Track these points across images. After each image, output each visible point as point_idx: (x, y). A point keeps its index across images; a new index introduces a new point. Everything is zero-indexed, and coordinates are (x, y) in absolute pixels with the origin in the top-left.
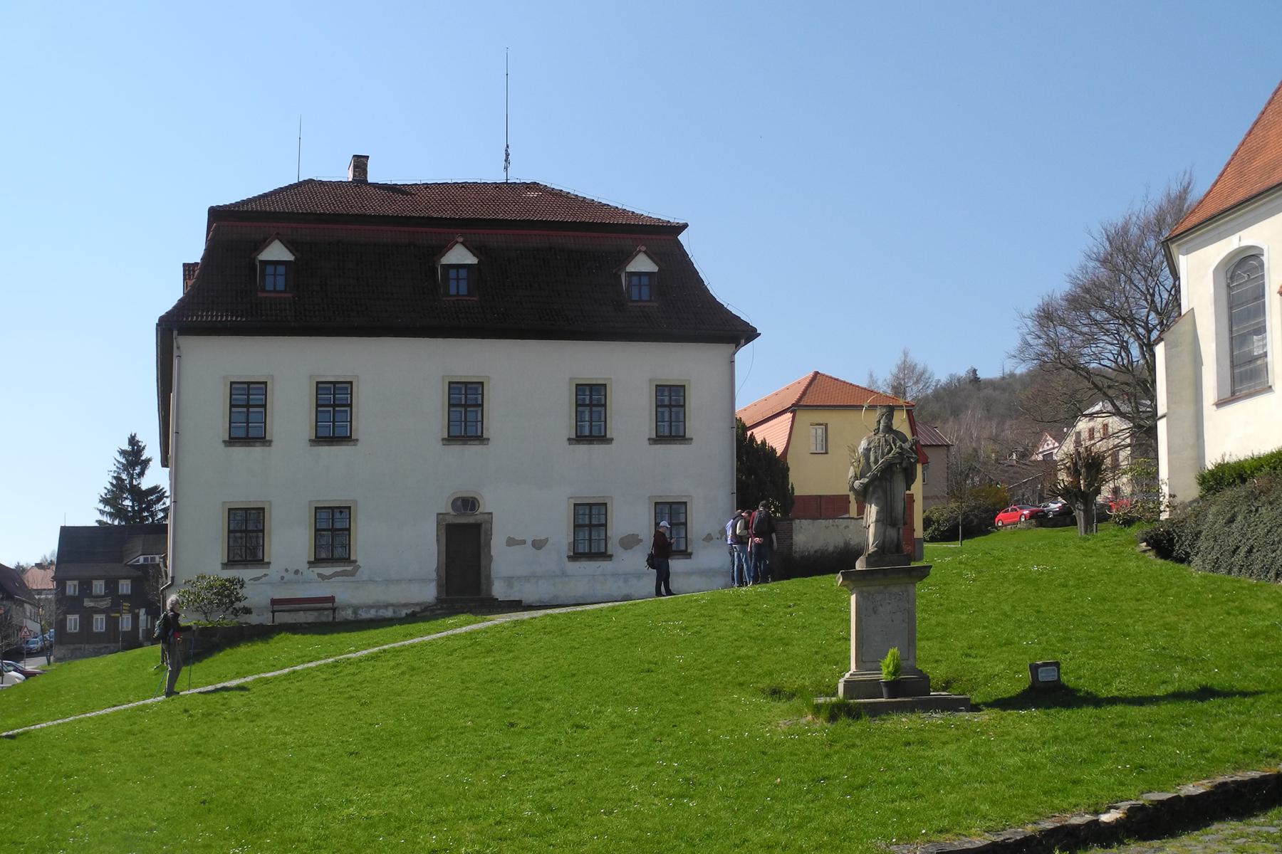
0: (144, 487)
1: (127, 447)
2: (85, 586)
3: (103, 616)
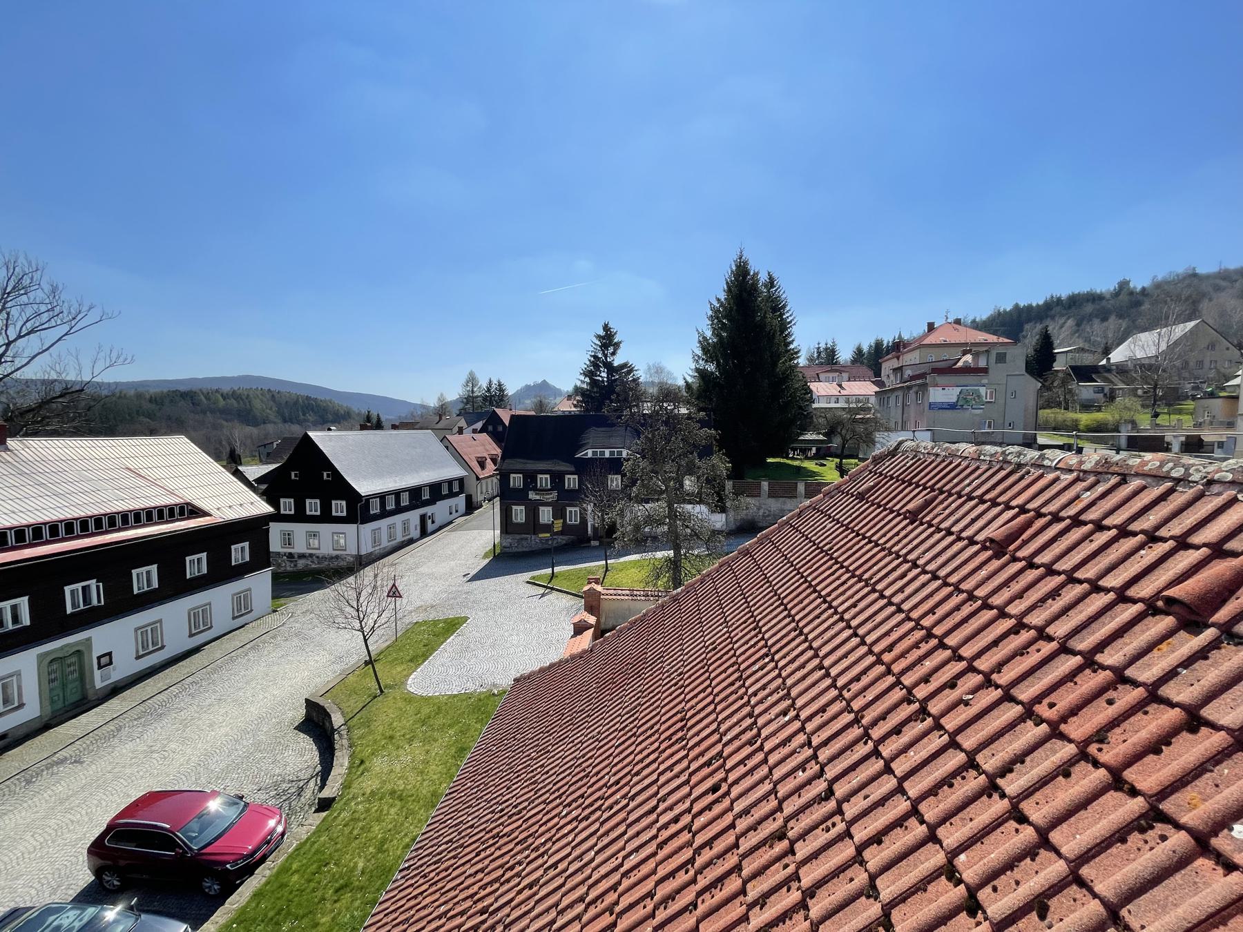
0: (616, 364)
1: (602, 333)
2: (530, 478)
3: (550, 509)
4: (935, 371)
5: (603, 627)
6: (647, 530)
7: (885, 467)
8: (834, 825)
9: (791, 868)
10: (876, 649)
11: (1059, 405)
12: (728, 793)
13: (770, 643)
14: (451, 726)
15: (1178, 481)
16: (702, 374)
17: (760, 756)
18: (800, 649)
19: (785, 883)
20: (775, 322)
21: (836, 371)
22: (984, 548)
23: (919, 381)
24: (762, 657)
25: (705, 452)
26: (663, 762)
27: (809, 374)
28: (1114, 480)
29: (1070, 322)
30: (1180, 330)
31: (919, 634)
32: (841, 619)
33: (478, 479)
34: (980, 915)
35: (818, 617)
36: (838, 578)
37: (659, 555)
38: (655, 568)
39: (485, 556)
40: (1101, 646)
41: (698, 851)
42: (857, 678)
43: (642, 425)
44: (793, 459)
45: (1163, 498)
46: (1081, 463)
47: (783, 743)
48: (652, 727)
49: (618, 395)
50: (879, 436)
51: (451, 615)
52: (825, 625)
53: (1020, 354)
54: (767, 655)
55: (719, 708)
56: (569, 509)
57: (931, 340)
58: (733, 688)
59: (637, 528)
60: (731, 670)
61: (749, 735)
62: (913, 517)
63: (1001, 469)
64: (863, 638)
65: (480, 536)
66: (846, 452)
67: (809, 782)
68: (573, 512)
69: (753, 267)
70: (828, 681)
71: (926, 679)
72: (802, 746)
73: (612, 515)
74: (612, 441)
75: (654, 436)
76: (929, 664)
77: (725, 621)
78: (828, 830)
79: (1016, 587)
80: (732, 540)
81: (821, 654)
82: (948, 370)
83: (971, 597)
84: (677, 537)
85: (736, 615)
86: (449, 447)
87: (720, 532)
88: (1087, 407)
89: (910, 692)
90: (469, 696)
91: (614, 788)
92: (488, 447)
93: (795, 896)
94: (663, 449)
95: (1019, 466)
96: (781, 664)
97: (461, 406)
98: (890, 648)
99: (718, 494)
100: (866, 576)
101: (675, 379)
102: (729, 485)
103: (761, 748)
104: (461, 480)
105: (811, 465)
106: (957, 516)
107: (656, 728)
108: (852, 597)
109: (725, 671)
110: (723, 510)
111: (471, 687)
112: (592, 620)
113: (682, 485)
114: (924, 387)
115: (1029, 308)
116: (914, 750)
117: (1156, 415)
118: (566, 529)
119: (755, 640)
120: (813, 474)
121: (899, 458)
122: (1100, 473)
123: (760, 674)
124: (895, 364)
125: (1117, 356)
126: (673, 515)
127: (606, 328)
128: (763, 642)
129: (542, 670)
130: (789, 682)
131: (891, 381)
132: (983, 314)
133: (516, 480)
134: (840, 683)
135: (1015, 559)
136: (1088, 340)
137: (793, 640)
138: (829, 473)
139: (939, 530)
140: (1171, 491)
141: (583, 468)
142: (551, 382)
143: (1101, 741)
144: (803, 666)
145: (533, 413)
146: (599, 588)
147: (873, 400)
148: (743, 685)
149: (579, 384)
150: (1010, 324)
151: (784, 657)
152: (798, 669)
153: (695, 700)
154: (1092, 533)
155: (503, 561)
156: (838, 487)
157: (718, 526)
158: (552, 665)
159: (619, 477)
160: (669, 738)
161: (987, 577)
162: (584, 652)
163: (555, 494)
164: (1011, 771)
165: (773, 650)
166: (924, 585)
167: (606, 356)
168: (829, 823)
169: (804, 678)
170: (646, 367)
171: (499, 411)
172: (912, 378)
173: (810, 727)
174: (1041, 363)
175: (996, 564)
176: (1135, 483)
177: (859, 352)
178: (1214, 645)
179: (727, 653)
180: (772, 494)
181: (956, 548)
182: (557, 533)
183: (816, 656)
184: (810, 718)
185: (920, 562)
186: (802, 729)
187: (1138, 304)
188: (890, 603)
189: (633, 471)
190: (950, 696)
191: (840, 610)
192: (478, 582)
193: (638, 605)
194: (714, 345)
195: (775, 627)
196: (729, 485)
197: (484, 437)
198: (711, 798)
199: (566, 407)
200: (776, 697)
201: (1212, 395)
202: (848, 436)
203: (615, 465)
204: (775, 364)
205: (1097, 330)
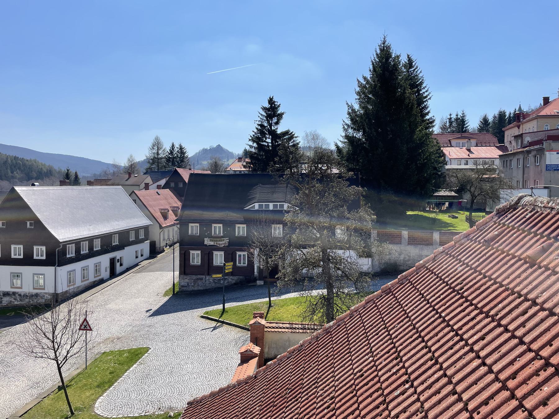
0: (279, 132)
1: (267, 105)
3: (222, 253)
5: (266, 356)
6: (304, 271)
10: (502, 376)
13: (410, 370)
16: (350, 140)
18: (436, 376)
23: (537, 147)
24: (403, 383)
27: (442, 140)
31: (538, 363)
32: (472, 350)
33: (161, 227)
35: (451, 348)
36: (468, 314)
37: (315, 293)
39: (166, 294)
50: (503, 193)
51: (134, 345)
54: (407, 381)
56: (238, 253)
58: (377, 411)
59: (296, 270)
65: (160, 278)
74: (275, 196)
75: (310, 192)
80: (377, 281)
81: (454, 380)
84: (330, 277)
85: (380, 346)
86: (137, 200)
87: (366, 274)
92: (171, 201)
94: (318, 202)
96: (419, 389)
97: (148, 166)
98: (513, 376)
101: (328, 144)
104: (146, 228)
108: (480, 330)
109: (370, 395)
112: (257, 350)
114: (541, 151)
119: (397, 368)
120: (447, 225)
124: (516, 132)
127: (271, 101)
128: (403, 370)
130: (427, 405)
131: (513, 146)
133: (194, 229)
134: (471, 406)
137: (430, 368)
144: (438, 392)
145: (209, 172)
146: (263, 322)
147: (497, 162)
148: (387, 408)
149: (248, 148)
151: (422, 383)
155: (181, 298)
158: (221, 390)
159: (281, 226)
162: (250, 378)
165: (413, 377)
166: (542, 321)
169: (439, 402)
171: (180, 170)
172: (531, 144)
177: (485, 121)
179: (372, 379)
182: (227, 274)
183: (450, 382)
188: (513, 337)
191: (470, 342)
194: (361, 116)
195: (414, 357)
197: (167, 191)
199: (238, 167)
204: (413, 132)
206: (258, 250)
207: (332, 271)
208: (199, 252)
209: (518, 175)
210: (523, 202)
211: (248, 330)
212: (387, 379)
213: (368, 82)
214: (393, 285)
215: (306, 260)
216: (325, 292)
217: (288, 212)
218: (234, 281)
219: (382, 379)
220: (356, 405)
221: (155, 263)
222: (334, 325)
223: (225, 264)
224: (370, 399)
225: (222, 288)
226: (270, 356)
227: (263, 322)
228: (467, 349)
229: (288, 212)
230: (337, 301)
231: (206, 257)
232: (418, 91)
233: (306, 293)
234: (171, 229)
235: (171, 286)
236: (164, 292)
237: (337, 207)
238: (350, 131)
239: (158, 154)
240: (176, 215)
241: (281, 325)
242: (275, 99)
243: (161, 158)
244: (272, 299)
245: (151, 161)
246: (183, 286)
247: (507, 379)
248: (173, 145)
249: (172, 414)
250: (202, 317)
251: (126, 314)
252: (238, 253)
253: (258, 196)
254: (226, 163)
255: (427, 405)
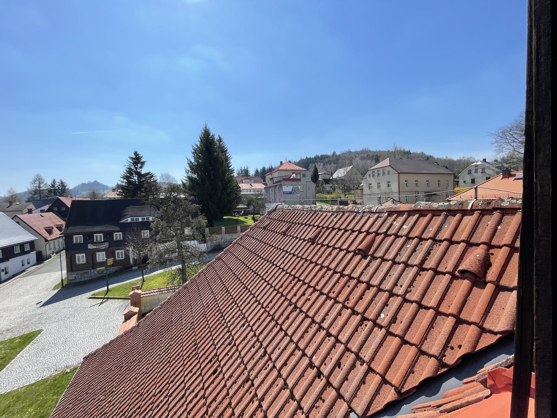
0: (143, 173)
1: (134, 156)
3: (104, 253)
4: (285, 180)
5: (143, 312)
6: (166, 256)
7: (272, 216)
8: (268, 365)
9: (253, 392)
10: (277, 288)
11: (321, 192)
12: (221, 371)
13: (234, 297)
14: (30, 406)
15: (356, 212)
16: (190, 179)
17: (235, 348)
18: (247, 296)
19: (252, 400)
20: (223, 157)
21: (249, 179)
22: (309, 242)
23: (279, 184)
24: (231, 304)
25: (195, 215)
26: (186, 370)
27: (238, 180)
28: (341, 214)
29: (322, 164)
30: (349, 168)
31: (291, 278)
32: (262, 279)
33: (46, 240)
34: (322, 376)
35: (253, 280)
36: (259, 262)
37: (174, 268)
38: (172, 275)
39: (55, 288)
40: (344, 269)
41: (209, 406)
42: (271, 302)
43: (161, 204)
44: (235, 216)
45: (354, 218)
46: (332, 209)
47: (244, 339)
48: (179, 354)
49: (145, 189)
50: (267, 205)
51: (26, 332)
52: (256, 283)
53: (309, 174)
54: (233, 302)
55: (213, 333)
56: (117, 252)
57: (281, 168)
58: (219, 322)
59: (161, 256)
60: (217, 313)
61: (228, 341)
62: (284, 234)
63: (311, 213)
64: (271, 284)
65: (54, 273)
66: (255, 212)
67: (257, 352)
68: (120, 254)
69: (212, 132)
70: (260, 306)
71: (295, 295)
72: (252, 337)
73: (146, 251)
74: (143, 212)
75: (167, 209)
76: (295, 288)
77: (212, 292)
78: (266, 368)
79: (319, 254)
80: (211, 255)
81: (256, 295)
82: (288, 179)
83: (306, 260)
84: (183, 257)
85: (217, 287)
86: (20, 222)
87: (204, 252)
88: (329, 193)
89: (290, 301)
90: (44, 381)
91: (159, 395)
92: (54, 220)
93: (256, 403)
94: (173, 215)
95: (316, 211)
96: (239, 305)
97: (30, 196)
98: (281, 286)
99: (203, 234)
100: (270, 260)
101: (177, 181)
102: (207, 230)
103: (235, 345)
104: (32, 243)
105: (242, 218)
106: (299, 231)
107: (181, 354)
108: (265, 269)
109: (214, 315)
110: (205, 242)
111: (47, 374)
112: (136, 310)
113: (184, 232)
114: (281, 185)
115: (310, 158)
116: (295, 324)
117: (345, 195)
118: (116, 263)
119: (227, 297)
120: (243, 222)
121: (277, 212)
122: (337, 212)
123: (231, 311)
124: (270, 177)
125: (335, 176)
126: (180, 247)
127: (136, 154)
128: (231, 297)
129: (105, 346)
130: (244, 311)
131: (270, 183)
132: (297, 160)
133: (78, 239)
134: (264, 306)
135: (318, 244)
136: (327, 170)
137: (244, 292)
138: (249, 221)
139: (293, 237)
140: (355, 216)
141: (125, 228)
142: (99, 181)
143: (348, 300)
144: (249, 303)
145: (89, 199)
146: (139, 292)
147: (263, 191)
148: (224, 319)
149: (120, 183)
150: (306, 163)
151: (241, 301)
152: (247, 304)
153: (201, 333)
154: (338, 232)
155: (67, 290)
156: (255, 225)
157: (203, 249)
158: (111, 342)
159: (148, 231)
160: (189, 357)
161: (310, 252)
162: (133, 328)
163: (107, 244)
164: (325, 319)
165: (235, 299)
166: (291, 259)
167: (136, 168)
168: (266, 366)
169: (250, 307)
170: (160, 175)
171: (62, 199)
172: (277, 182)
173: (254, 328)
174: (315, 177)
175: (312, 247)
176: (347, 214)
177: (257, 171)
178: (370, 261)
179: (214, 306)
180: (227, 232)
181: (299, 243)
182: (110, 266)
183: (254, 297)
184: (254, 324)
185: (288, 251)
186: (252, 330)
187: (338, 160)
188: (280, 269)
189: (157, 228)
190: (304, 298)
191: (261, 275)
192: (50, 306)
193: (163, 296)
194: (195, 166)
195: (235, 289)
196: (207, 230)
197: (51, 214)
198: (213, 377)
199: (113, 195)
200: (239, 319)
201: (357, 189)
202: (255, 206)
203: (146, 225)
204: (224, 175)
205: (330, 167)
206: (132, 247)
207: (184, 254)
208: (84, 254)
209: (272, 196)
210: (278, 208)
211: (129, 299)
212: (222, 304)
213: (198, 147)
214: (221, 255)
215: (167, 249)
216: (180, 266)
217: (153, 222)
218: (115, 270)
219: (220, 305)
220: (207, 322)
221: (42, 267)
222: (189, 283)
223: (106, 260)
224: (214, 317)
225: (105, 276)
226: (146, 311)
227: (139, 292)
228: (260, 279)
229: (153, 222)
230: (188, 270)
231: (91, 257)
232: (225, 154)
233: (167, 269)
234: (56, 241)
235: (60, 281)
236: (53, 287)
237: (185, 217)
238: (190, 173)
239: (39, 187)
240: (60, 231)
241: (152, 291)
242: (138, 153)
243: (43, 190)
244: (144, 276)
245: (33, 192)
246: (71, 280)
247: (279, 288)
248: (54, 181)
249: (69, 371)
250: (90, 298)
251: (15, 310)
252: (117, 252)
253: (130, 213)
254: (103, 193)
255: (244, 311)
